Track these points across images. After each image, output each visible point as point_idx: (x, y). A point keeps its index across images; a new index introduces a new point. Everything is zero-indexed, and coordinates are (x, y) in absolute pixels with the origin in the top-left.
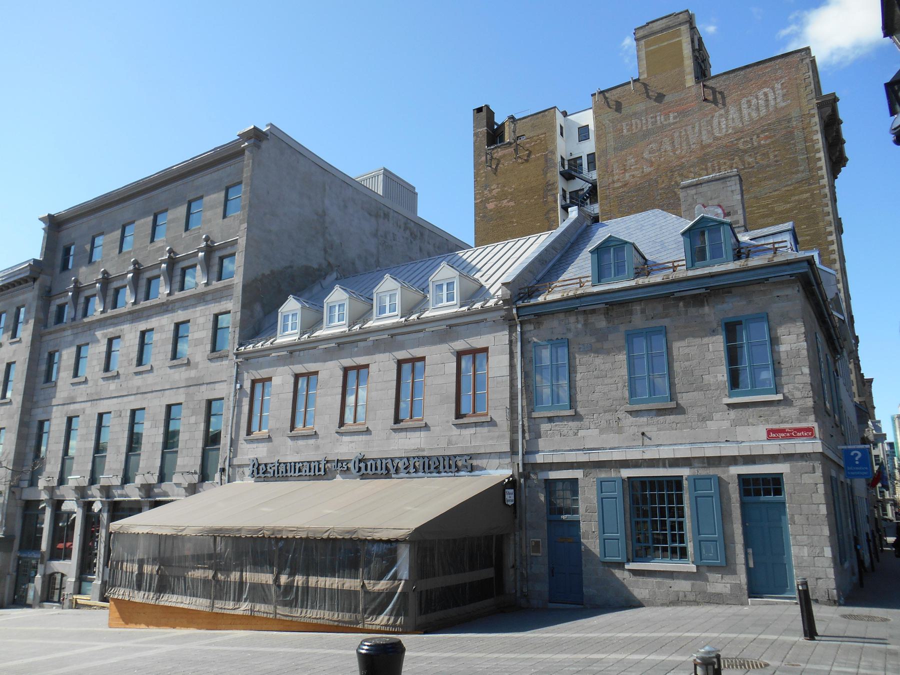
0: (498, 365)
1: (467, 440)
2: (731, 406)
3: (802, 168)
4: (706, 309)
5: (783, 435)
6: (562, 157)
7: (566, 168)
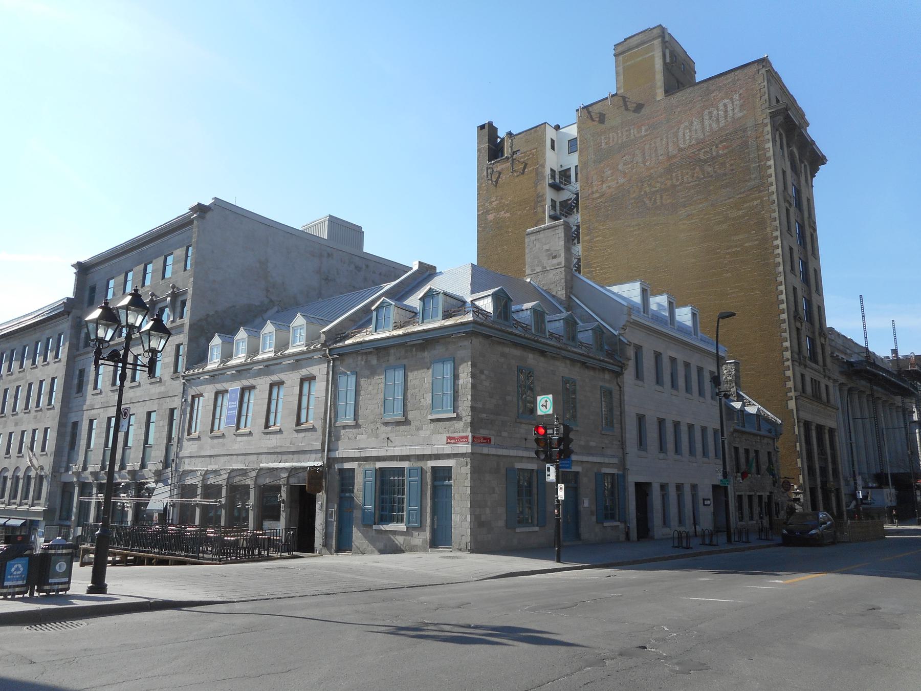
0: (319, 389)
2: (433, 420)
3: (753, 176)
4: (426, 354)
7: (557, 181)
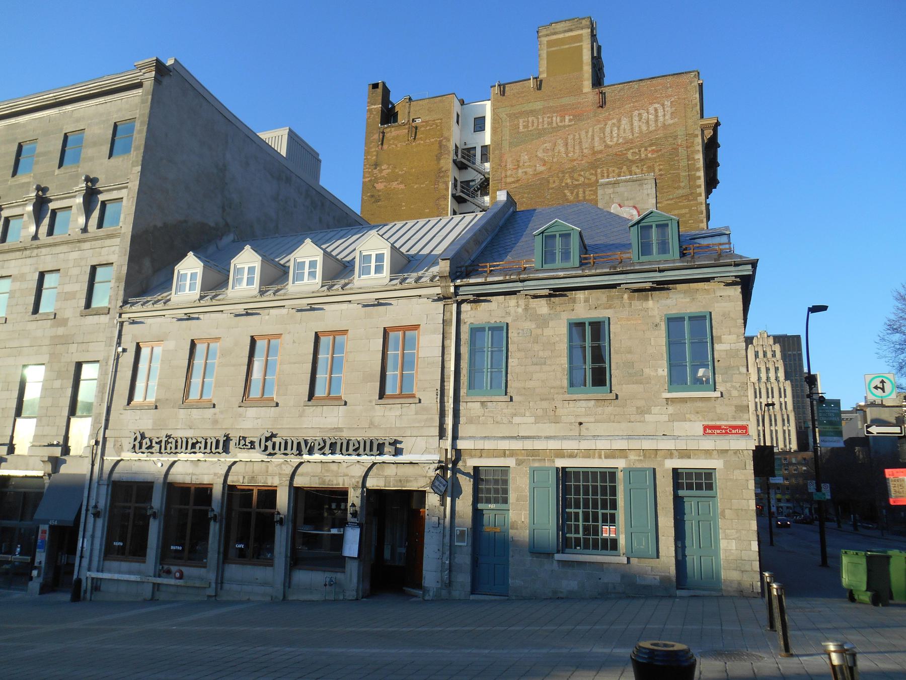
1: (388, 420)
5: (719, 431)
6: (456, 146)
